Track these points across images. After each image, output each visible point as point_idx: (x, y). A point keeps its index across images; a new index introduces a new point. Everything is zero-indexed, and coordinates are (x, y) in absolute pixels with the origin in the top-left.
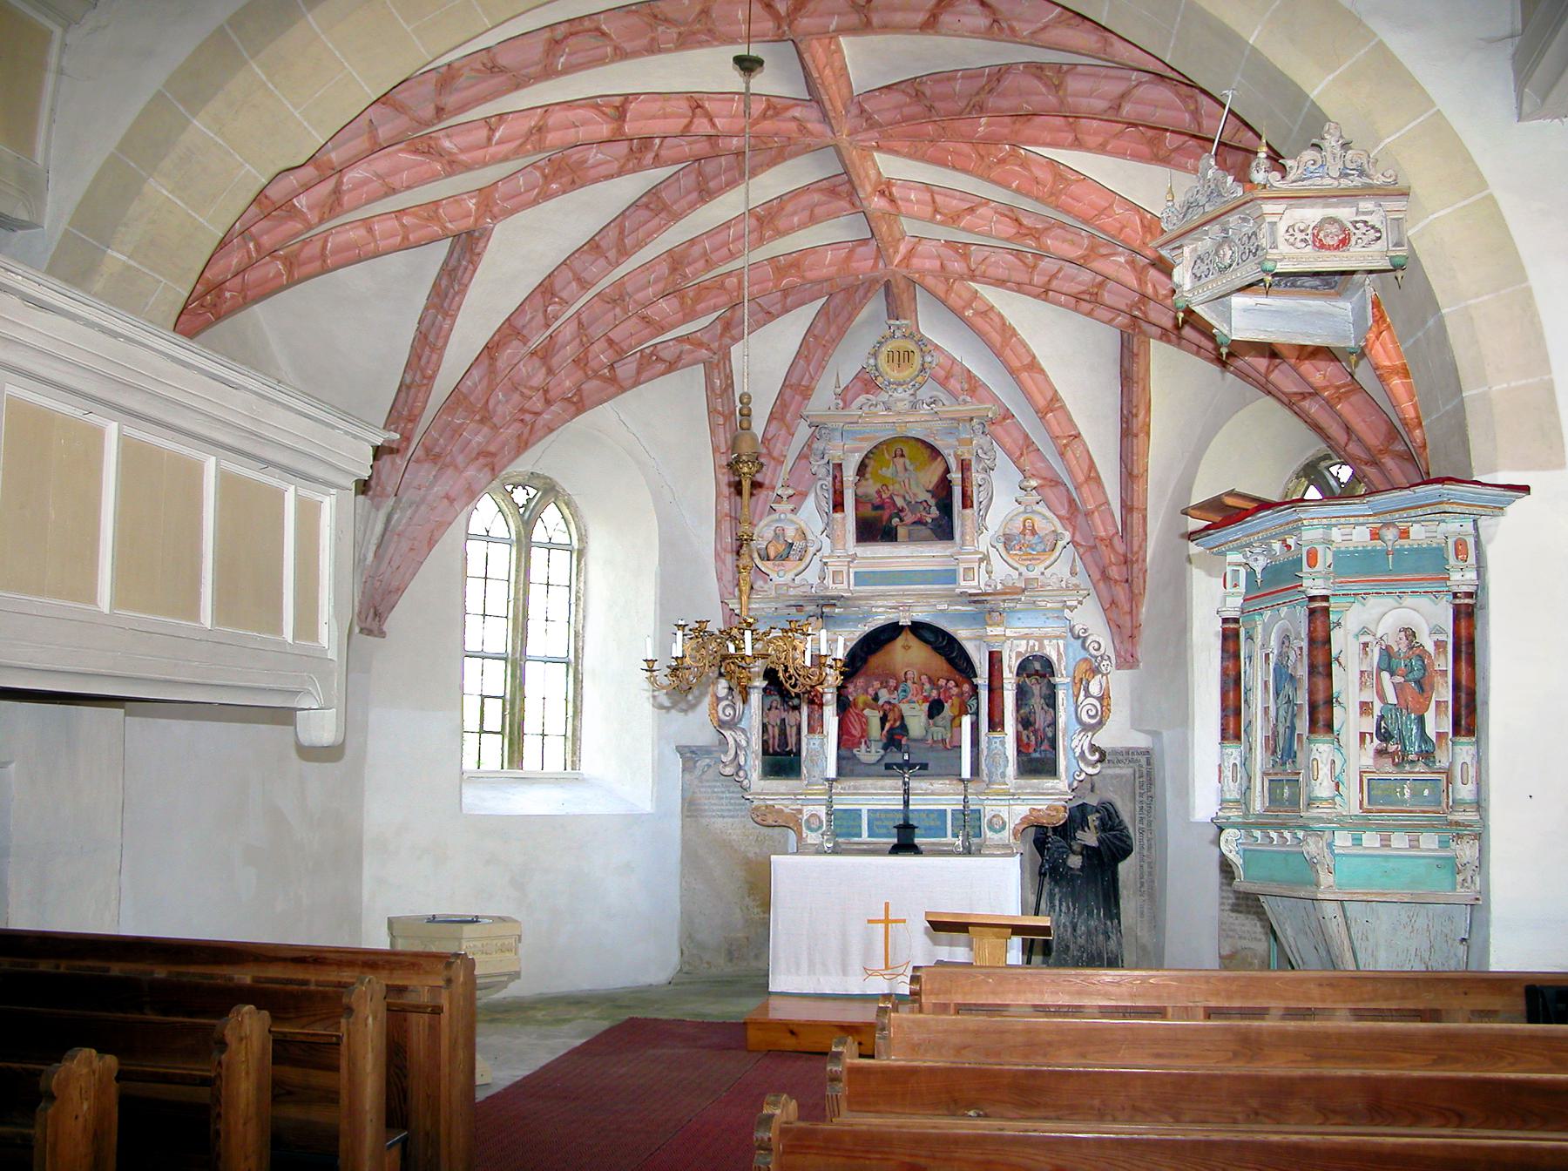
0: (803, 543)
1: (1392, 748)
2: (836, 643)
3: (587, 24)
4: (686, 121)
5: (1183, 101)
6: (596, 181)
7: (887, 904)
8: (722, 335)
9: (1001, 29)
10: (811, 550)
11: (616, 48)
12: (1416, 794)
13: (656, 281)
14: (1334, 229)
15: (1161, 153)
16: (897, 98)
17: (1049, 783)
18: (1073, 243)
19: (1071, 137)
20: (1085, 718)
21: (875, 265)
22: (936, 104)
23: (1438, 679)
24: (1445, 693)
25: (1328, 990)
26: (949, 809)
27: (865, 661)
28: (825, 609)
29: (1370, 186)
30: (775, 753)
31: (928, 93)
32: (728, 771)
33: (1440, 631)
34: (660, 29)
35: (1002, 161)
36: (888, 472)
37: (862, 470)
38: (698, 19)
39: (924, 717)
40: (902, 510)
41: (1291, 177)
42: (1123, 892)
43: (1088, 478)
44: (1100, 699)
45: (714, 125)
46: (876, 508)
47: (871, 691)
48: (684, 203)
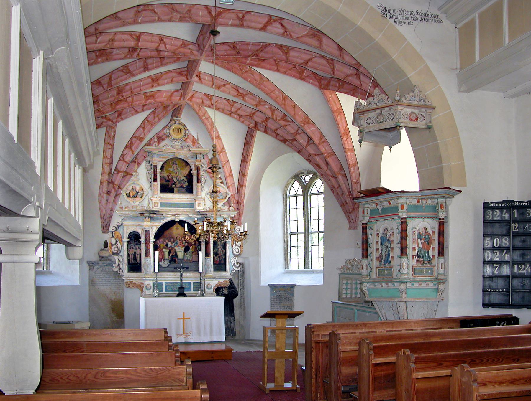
0: (142, 192)
1: (421, 260)
2: (153, 227)
3: (150, 7)
4: (158, 44)
5: (329, 65)
6: (115, 60)
7: (184, 313)
8: (118, 117)
9: (287, 35)
10: (145, 194)
11: (159, 18)
12: (427, 272)
13: (111, 97)
14: (414, 115)
15: (302, 77)
16: (226, 47)
17: (224, 273)
18: (254, 100)
19: (276, 68)
20: (235, 253)
21: (180, 99)
22: (241, 52)
23: (433, 241)
24: (436, 245)
25: (416, 324)
26: (192, 282)
27: (163, 233)
28: (152, 214)
29: (426, 105)
30: (132, 264)
31: (238, 47)
32: (116, 270)
33: (434, 228)
34: (175, 14)
35: (246, 72)
36: (171, 169)
37: (162, 168)
38: (187, 13)
39: (183, 252)
40: (176, 182)
41: (407, 99)
42: (235, 308)
43: (230, 175)
44: (240, 247)
45: (166, 47)
46: (167, 181)
47: (165, 243)
48: (137, 71)
